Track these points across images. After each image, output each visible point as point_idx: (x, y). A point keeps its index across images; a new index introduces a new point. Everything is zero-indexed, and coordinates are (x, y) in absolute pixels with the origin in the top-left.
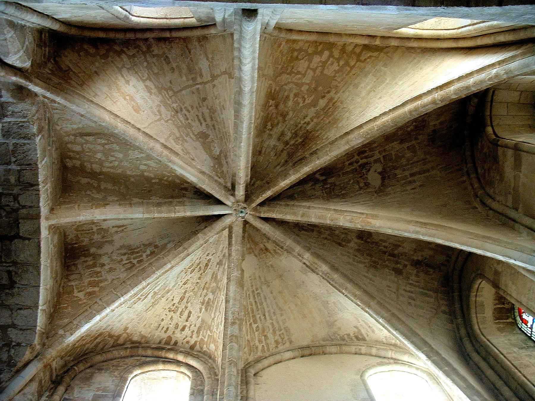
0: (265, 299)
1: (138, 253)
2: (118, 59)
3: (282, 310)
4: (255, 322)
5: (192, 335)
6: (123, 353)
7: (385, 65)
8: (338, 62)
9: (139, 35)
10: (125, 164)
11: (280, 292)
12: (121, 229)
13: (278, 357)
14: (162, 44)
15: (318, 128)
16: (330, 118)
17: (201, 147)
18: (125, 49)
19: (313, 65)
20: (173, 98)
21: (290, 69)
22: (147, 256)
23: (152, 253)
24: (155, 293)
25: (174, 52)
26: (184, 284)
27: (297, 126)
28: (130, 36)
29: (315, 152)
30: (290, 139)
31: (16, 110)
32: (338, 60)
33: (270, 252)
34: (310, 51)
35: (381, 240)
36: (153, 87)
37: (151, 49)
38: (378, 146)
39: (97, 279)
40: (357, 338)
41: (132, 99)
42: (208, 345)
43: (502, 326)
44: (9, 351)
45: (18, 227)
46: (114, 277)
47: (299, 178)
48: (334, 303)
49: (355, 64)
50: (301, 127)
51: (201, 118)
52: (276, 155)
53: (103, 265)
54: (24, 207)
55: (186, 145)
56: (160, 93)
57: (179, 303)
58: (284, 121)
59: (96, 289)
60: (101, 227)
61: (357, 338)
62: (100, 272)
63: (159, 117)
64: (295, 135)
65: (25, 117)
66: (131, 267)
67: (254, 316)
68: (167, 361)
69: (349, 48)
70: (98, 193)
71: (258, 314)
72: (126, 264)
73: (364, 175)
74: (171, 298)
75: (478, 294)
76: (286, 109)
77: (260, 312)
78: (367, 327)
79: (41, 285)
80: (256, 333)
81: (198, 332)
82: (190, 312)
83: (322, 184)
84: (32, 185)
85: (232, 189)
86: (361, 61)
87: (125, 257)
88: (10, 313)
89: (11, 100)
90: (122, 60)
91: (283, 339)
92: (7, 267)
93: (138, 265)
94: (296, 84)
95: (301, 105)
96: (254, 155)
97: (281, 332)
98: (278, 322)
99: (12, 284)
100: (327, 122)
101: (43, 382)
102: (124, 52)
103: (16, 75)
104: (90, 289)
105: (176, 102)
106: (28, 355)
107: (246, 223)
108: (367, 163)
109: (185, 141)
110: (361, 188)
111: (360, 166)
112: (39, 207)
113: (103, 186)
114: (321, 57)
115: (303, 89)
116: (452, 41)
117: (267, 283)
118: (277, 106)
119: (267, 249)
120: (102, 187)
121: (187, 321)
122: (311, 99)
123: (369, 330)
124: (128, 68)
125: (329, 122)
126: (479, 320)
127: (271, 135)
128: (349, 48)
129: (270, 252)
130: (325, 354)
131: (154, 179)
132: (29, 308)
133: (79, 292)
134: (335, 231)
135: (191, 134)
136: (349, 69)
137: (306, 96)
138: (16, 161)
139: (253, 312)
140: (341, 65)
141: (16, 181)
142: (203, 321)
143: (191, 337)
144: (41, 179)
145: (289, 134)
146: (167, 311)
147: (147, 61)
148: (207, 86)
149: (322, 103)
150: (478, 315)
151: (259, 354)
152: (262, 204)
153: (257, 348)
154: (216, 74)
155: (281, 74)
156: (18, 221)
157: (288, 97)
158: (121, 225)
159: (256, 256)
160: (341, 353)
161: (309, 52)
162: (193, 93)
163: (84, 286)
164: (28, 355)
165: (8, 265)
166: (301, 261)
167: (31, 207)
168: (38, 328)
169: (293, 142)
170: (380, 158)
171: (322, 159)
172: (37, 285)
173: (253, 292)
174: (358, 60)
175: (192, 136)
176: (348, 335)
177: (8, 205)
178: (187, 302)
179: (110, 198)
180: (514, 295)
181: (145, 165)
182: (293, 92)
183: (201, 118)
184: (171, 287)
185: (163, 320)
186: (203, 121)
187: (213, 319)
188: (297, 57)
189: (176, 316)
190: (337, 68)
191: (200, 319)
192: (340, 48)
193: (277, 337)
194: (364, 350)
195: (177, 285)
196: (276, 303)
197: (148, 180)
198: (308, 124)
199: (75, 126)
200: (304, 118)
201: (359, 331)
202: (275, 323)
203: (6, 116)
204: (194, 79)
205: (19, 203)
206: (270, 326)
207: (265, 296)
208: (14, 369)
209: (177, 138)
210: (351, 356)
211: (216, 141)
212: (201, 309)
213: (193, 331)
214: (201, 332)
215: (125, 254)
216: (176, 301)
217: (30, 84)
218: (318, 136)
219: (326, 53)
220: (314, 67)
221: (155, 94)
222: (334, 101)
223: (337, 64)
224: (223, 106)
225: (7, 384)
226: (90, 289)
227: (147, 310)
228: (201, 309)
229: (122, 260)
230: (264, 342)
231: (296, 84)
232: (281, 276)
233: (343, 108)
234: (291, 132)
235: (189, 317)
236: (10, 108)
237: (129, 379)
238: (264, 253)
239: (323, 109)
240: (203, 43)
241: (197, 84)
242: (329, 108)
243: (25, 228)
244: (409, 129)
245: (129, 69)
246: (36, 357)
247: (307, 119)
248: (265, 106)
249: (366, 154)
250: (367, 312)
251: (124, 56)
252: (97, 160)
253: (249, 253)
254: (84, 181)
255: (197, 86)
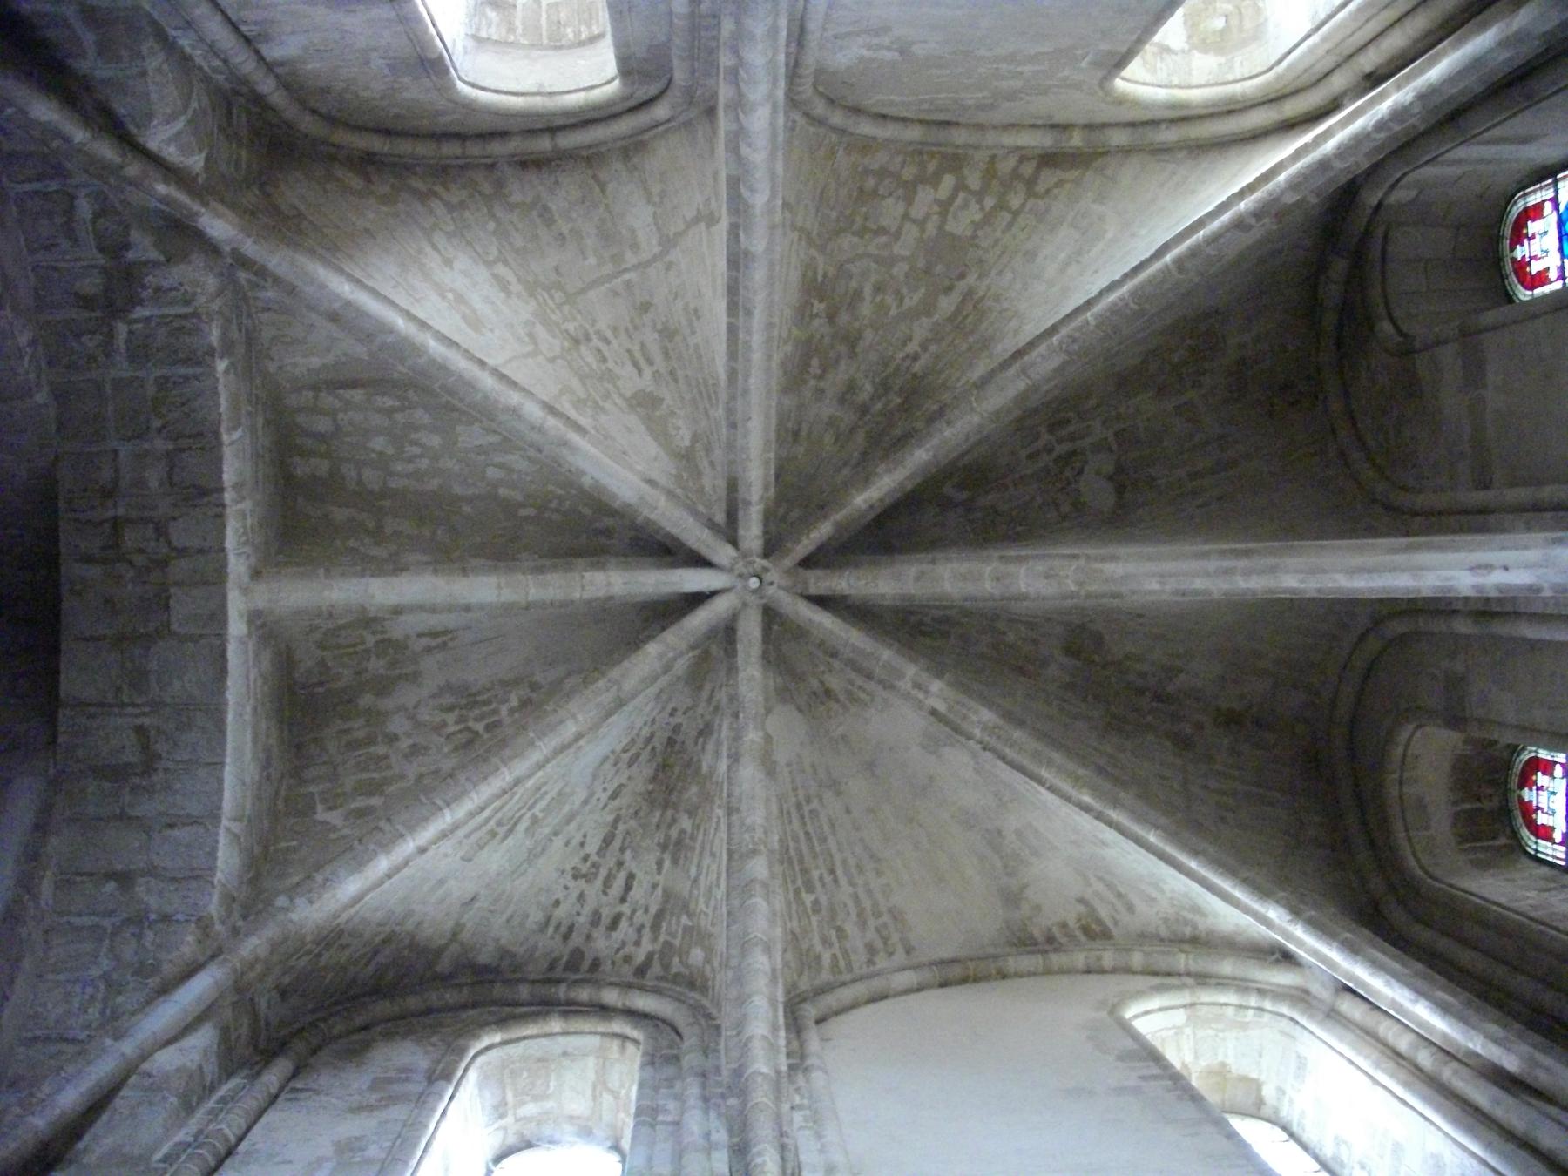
0: (832, 826)
1: (487, 703)
2: (420, 208)
3: (878, 860)
4: (810, 888)
5: (640, 937)
6: (451, 997)
7: (1101, 198)
8: (980, 201)
9: (474, 149)
10: (449, 463)
11: (871, 811)
12: (439, 640)
13: (877, 984)
14: (532, 176)
15: (941, 365)
16: (971, 339)
17: (643, 428)
18: (438, 189)
19: (917, 211)
20: (566, 308)
21: (859, 220)
22: (512, 711)
23: (525, 703)
24: (535, 821)
25: (564, 193)
26: (614, 796)
27: (886, 365)
28: (451, 149)
29: (941, 413)
30: (872, 399)
31: (165, 284)
32: (980, 195)
33: (837, 701)
34: (909, 173)
35: (1127, 657)
36: (512, 278)
37: (506, 191)
38: (1098, 406)
39: (375, 775)
40: (1086, 930)
41: (460, 299)
42: (683, 953)
43: (1481, 856)
44: (139, 937)
45: (167, 607)
46: (423, 769)
47: (901, 484)
48: (1018, 833)
49: (1023, 205)
50: (898, 369)
51: (638, 355)
52: (836, 440)
53: (393, 739)
54: (182, 552)
55: (603, 418)
56: (532, 295)
57: (601, 852)
58: (853, 354)
59: (375, 801)
60: (386, 636)
61: (1086, 930)
62: (386, 757)
63: (530, 348)
64: (884, 387)
65: (187, 303)
66: (470, 742)
67: (804, 871)
68: (571, 1009)
69: (1006, 166)
70: (377, 544)
71: (817, 868)
72: (453, 734)
73: (1069, 483)
74: (578, 838)
75: (1406, 775)
76: (857, 325)
77: (820, 860)
78: (1111, 897)
79: (228, 760)
80: (814, 919)
81: (656, 927)
82: (631, 877)
83: (960, 510)
84: (203, 492)
85: (729, 532)
86: (1036, 196)
87: (450, 718)
88: (144, 836)
89: (154, 254)
90: (432, 212)
91: (885, 940)
92: (137, 716)
93: (486, 736)
94: (878, 260)
95: (893, 312)
96: (780, 441)
97: (880, 921)
98: (869, 892)
99: (150, 762)
100: (964, 347)
101: (233, 1038)
102: (435, 194)
103: (166, 181)
104: (360, 803)
105: (575, 319)
106: (188, 945)
107: (770, 615)
108: (1074, 453)
109: (598, 408)
110: (1065, 518)
111: (1056, 461)
112: (223, 550)
113: (390, 525)
114: (936, 190)
115: (895, 271)
116: (1266, 106)
117: (835, 786)
118: (831, 317)
119: (828, 693)
120: (388, 530)
121: (623, 900)
122: (917, 297)
123: (1119, 905)
124: (447, 233)
125: (970, 349)
126: (1418, 847)
127: (823, 391)
128: (1006, 166)
129: (837, 701)
130: (1004, 976)
131: (522, 505)
132: (195, 821)
133: (330, 809)
134: (1004, 633)
135: (615, 396)
136: (1007, 217)
137: (905, 291)
138: (164, 427)
139: (801, 861)
140: (987, 209)
141: (161, 485)
142: (668, 895)
143: (637, 943)
144: (228, 477)
145: (869, 387)
146: (569, 877)
147: (493, 216)
148: (652, 271)
149: (947, 304)
150: (1412, 833)
151: (825, 976)
152: (807, 562)
153: (818, 958)
154: (671, 234)
155: (838, 232)
156: (167, 591)
157: (858, 295)
158: (440, 629)
159: (800, 710)
160: (1048, 972)
161: (905, 178)
162: (616, 294)
163: (344, 794)
164: (188, 945)
165: (137, 711)
166: (920, 705)
167: (201, 551)
168: (219, 875)
169: (879, 406)
170: (1106, 439)
171: (959, 424)
172: (215, 760)
173: (799, 806)
174: (1031, 193)
175: (619, 401)
176: (1064, 925)
177: (141, 551)
178: (622, 850)
179: (411, 558)
180: (1511, 717)
181: (501, 466)
182: (872, 280)
183: (638, 355)
184: (578, 803)
185: (557, 903)
186: (643, 363)
187: (695, 881)
188: (875, 192)
189: (593, 890)
190: (978, 217)
191: (659, 891)
192: (983, 166)
193: (871, 935)
194: (1108, 959)
195: (593, 801)
196: (862, 840)
197: (509, 508)
198: (915, 358)
199: (315, 362)
200: (904, 344)
201: (1093, 910)
202: (862, 896)
203: (141, 302)
204: (617, 259)
205: (169, 543)
206: (850, 903)
207: (830, 820)
208: (154, 982)
209: (579, 401)
210: (1079, 977)
211: (681, 413)
212: (660, 864)
213: (643, 926)
214: (664, 925)
215: (451, 709)
216: (592, 847)
217: (203, 210)
218: (944, 384)
219: (948, 181)
220: (920, 216)
221: (519, 296)
222: (976, 297)
223: (978, 206)
224: (696, 311)
225: (134, 1019)
226: (360, 803)
227: (513, 872)
228: (660, 864)
229: (444, 724)
230: (837, 945)
231: (878, 260)
232: (870, 766)
233: (1000, 312)
234: (873, 382)
235: (628, 887)
236: (150, 278)
237: (472, 1052)
238: (822, 703)
239: (951, 319)
240: (635, 160)
241: (626, 270)
242: (967, 316)
243: (184, 606)
244: (1176, 358)
245: (449, 235)
246: (213, 957)
247: (912, 347)
248: (803, 313)
249: (1071, 428)
250: (1110, 824)
251: (436, 205)
252: (373, 455)
253: (783, 700)
254: (340, 514)
255: (627, 276)
